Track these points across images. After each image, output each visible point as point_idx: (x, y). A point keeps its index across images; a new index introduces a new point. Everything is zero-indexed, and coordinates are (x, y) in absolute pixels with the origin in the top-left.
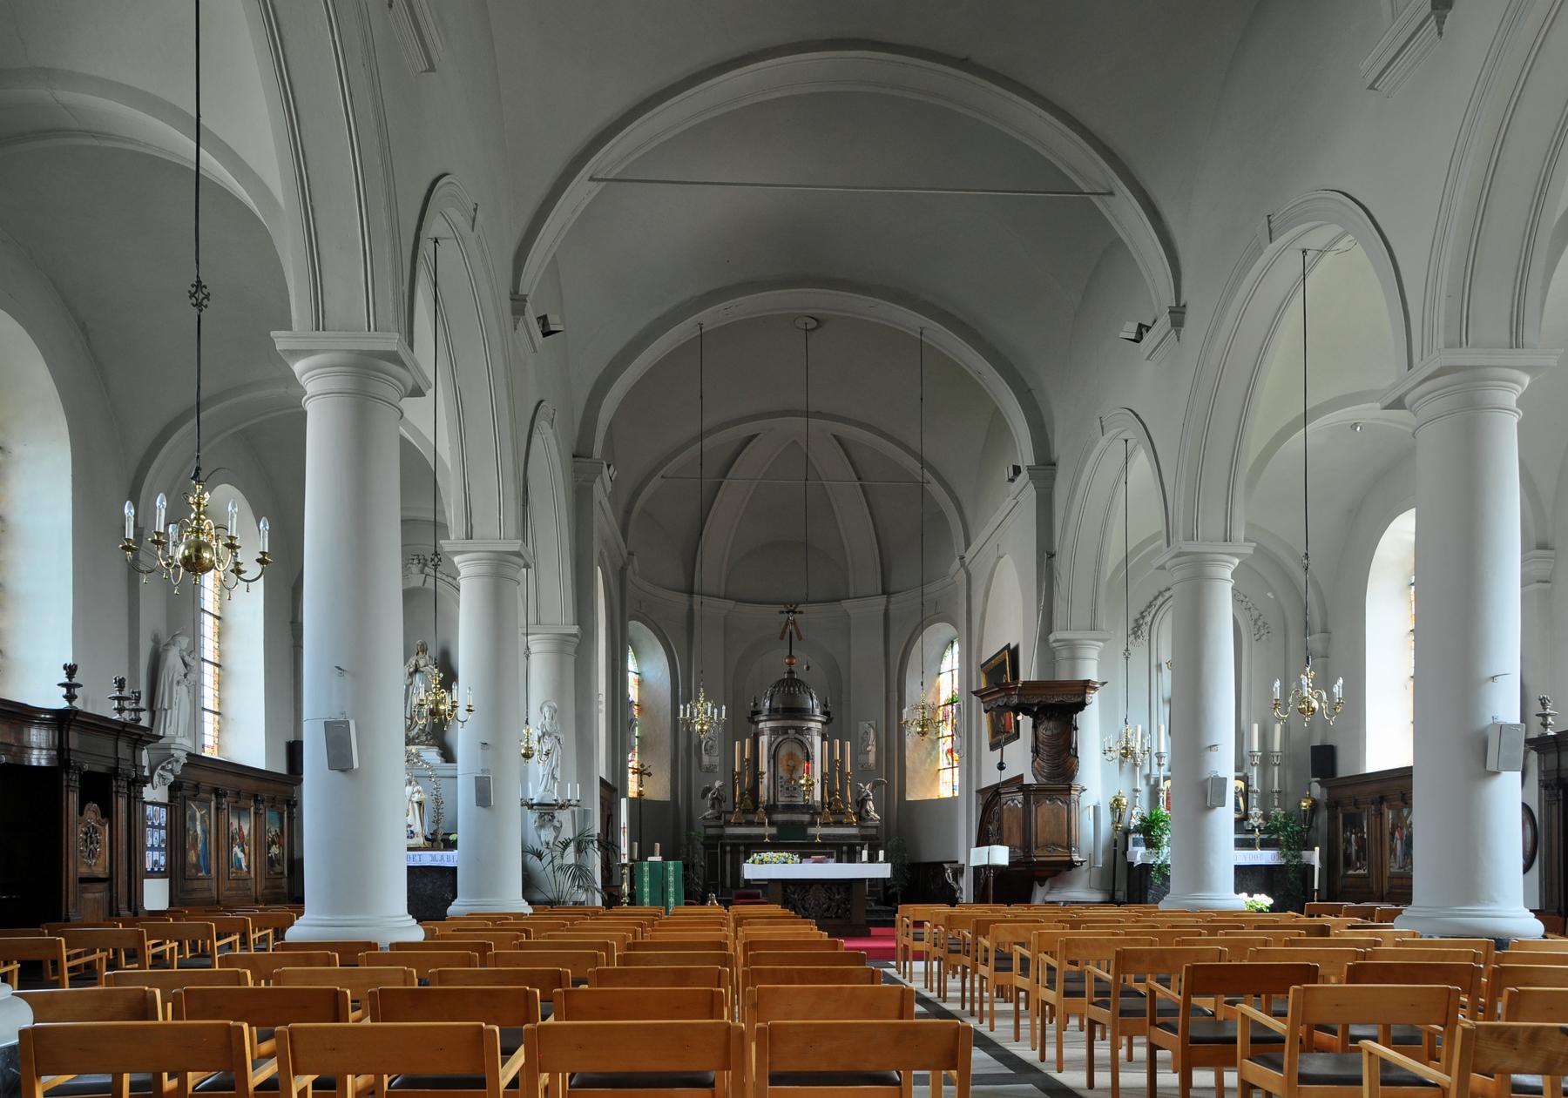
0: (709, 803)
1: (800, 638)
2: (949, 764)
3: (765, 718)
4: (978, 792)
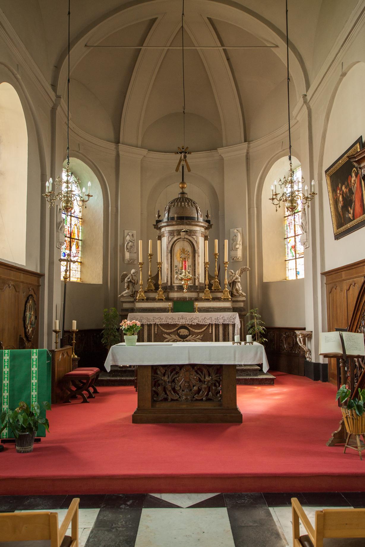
0: (126, 285)
1: (189, 170)
3: (165, 224)
4: (322, 274)
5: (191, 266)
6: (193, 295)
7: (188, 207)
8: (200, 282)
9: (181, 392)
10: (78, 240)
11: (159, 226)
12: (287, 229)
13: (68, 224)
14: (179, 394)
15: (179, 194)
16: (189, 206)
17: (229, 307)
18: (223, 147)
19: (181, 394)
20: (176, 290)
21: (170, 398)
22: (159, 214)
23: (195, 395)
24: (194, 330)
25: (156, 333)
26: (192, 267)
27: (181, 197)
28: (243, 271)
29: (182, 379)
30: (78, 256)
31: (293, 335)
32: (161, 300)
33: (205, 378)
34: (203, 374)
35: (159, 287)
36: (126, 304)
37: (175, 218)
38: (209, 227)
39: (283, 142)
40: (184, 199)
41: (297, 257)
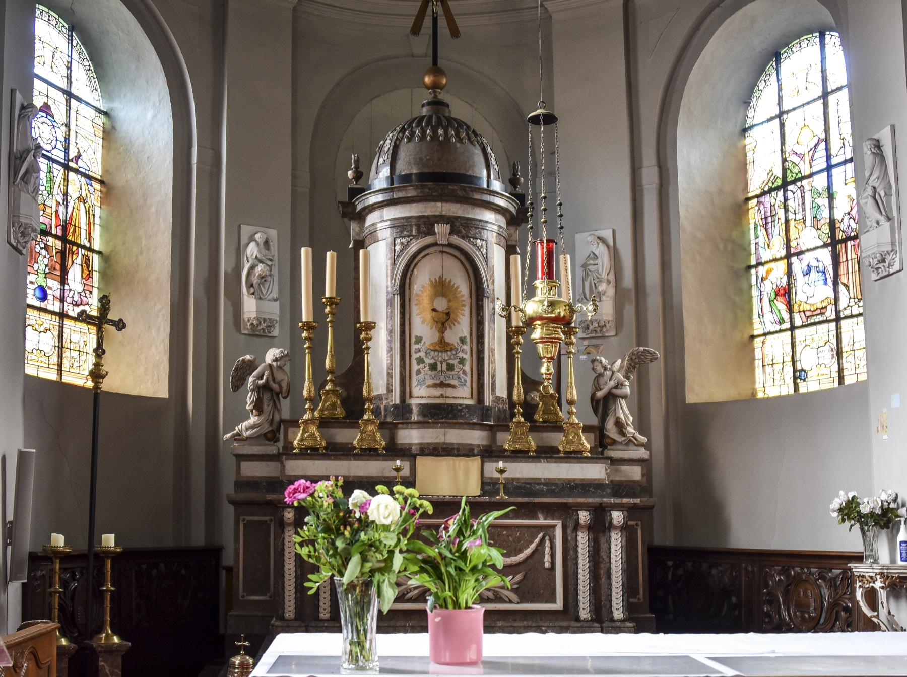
0: (250, 399)
1: (455, 32)
2: (781, 321)
3: (380, 198)
5: (468, 340)
7: (458, 145)
8: (498, 394)
11: (359, 207)
12: (757, 237)
13: (55, 192)
16: (460, 140)
17: (599, 479)
20: (415, 417)
22: (357, 168)
27: (430, 113)
30: (88, 304)
32: (369, 453)
41: (798, 322)
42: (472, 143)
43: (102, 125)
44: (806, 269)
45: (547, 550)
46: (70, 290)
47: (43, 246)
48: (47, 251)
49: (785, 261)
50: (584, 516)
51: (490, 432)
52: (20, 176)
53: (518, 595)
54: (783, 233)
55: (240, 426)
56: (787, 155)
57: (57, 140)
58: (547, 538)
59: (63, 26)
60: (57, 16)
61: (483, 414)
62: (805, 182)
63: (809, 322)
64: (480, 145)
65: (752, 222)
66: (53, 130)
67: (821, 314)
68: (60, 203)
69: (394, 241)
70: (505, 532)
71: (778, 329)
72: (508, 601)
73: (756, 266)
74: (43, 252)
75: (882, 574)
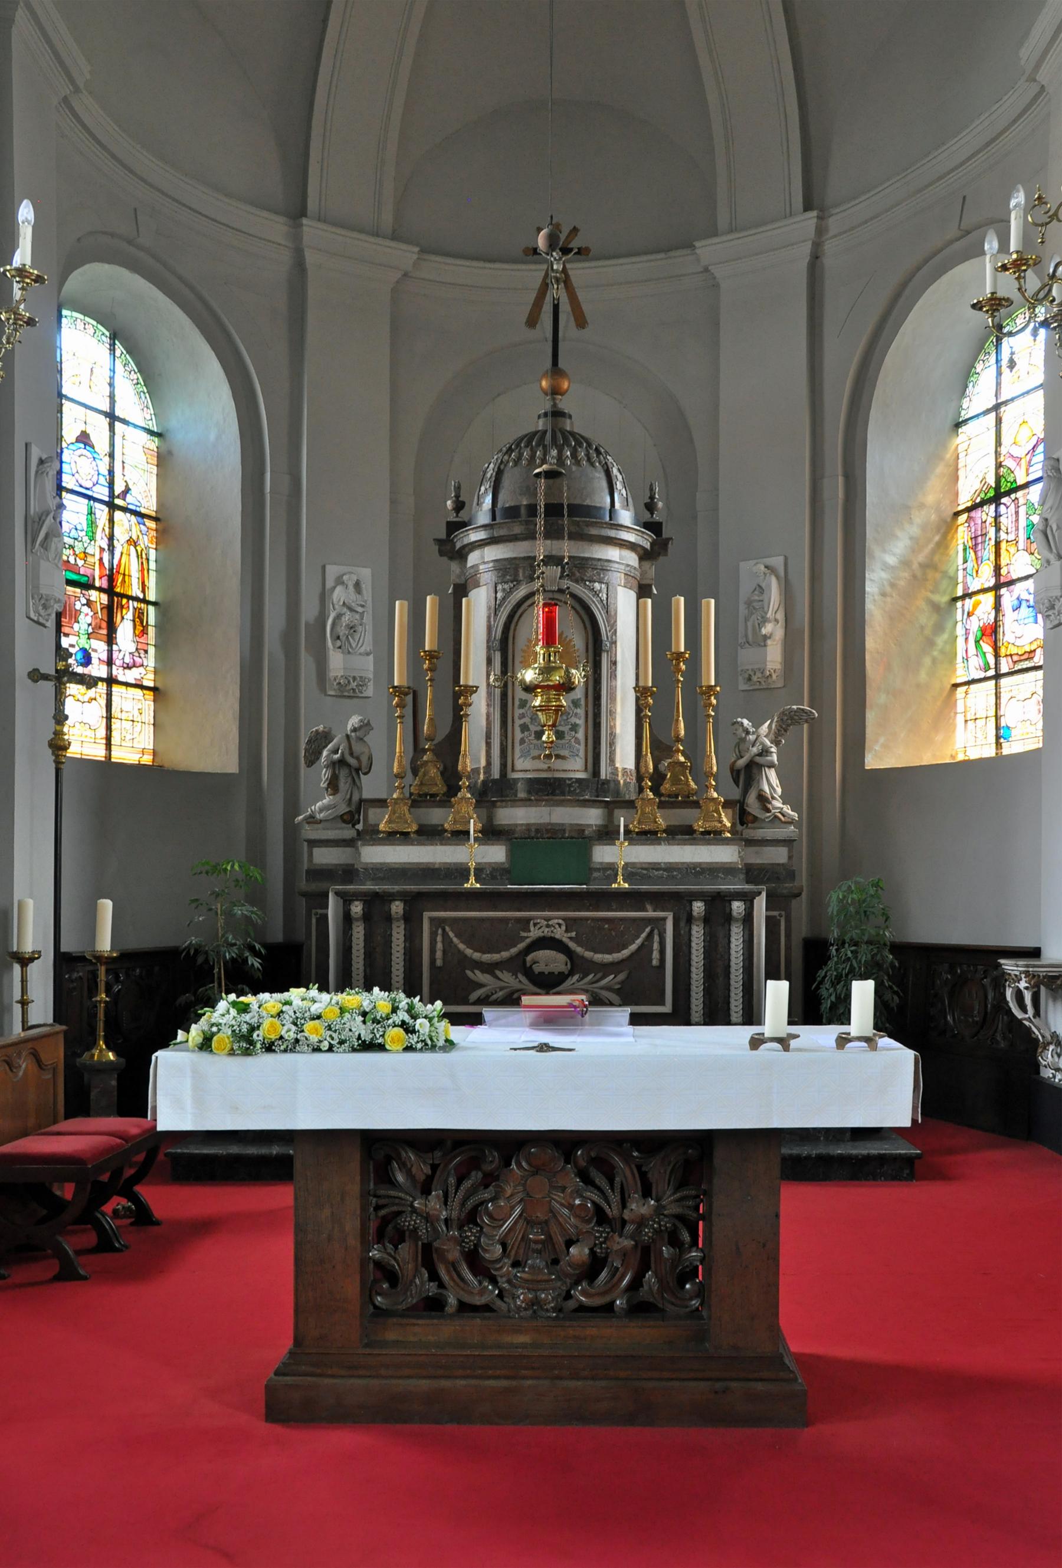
0: (325, 775)
1: (581, 321)
2: (987, 668)
3: (481, 535)
5: (583, 702)
6: (592, 817)
7: (574, 468)
9: (508, 1273)
10: (144, 601)
11: (458, 545)
12: (965, 561)
14: (499, 1279)
15: (539, 417)
16: (577, 462)
18: (715, 234)
19: (509, 1282)
20: (522, 795)
21: (452, 1300)
22: (457, 496)
23: (577, 1283)
24: (588, 954)
25: (439, 963)
26: (586, 705)
28: (787, 722)
29: (512, 1208)
30: (142, 665)
31: (986, 978)
33: (624, 1205)
34: (617, 1185)
35: (458, 785)
36: (324, 850)
37: (523, 511)
38: (656, 548)
39: (964, 198)
40: (559, 435)
41: (1004, 668)
42: (592, 464)
43: (156, 450)
44: (1016, 603)
45: (656, 946)
46: (120, 651)
47: (84, 601)
48: (89, 607)
49: (993, 593)
50: (698, 907)
51: (606, 810)
52: (38, 542)
53: (620, 996)
54: (992, 558)
55: (313, 808)
56: (1002, 459)
57: (99, 474)
58: (656, 931)
59: (103, 334)
60: (95, 323)
61: (597, 788)
62: (1020, 494)
63: (1016, 669)
64: (603, 466)
65: (960, 542)
66: (94, 463)
67: (1030, 659)
68: (104, 549)
69: (496, 587)
70: (606, 926)
71: (982, 677)
72: (608, 1002)
73: (963, 597)
74: (86, 609)
75: (1027, 973)
